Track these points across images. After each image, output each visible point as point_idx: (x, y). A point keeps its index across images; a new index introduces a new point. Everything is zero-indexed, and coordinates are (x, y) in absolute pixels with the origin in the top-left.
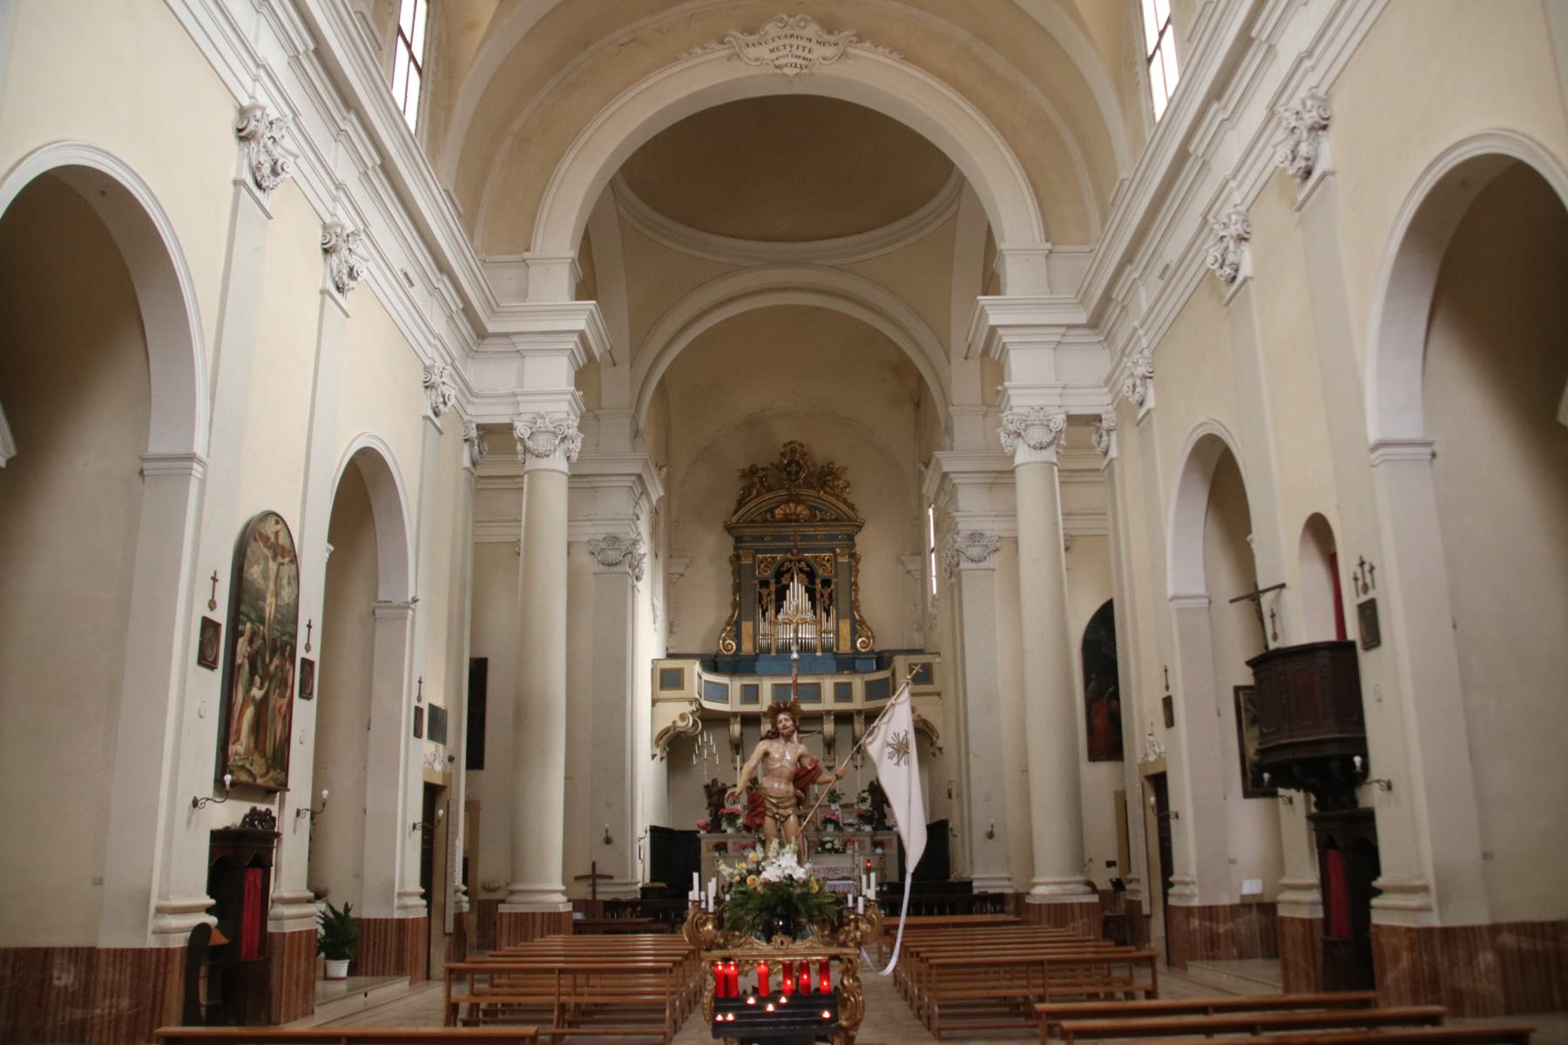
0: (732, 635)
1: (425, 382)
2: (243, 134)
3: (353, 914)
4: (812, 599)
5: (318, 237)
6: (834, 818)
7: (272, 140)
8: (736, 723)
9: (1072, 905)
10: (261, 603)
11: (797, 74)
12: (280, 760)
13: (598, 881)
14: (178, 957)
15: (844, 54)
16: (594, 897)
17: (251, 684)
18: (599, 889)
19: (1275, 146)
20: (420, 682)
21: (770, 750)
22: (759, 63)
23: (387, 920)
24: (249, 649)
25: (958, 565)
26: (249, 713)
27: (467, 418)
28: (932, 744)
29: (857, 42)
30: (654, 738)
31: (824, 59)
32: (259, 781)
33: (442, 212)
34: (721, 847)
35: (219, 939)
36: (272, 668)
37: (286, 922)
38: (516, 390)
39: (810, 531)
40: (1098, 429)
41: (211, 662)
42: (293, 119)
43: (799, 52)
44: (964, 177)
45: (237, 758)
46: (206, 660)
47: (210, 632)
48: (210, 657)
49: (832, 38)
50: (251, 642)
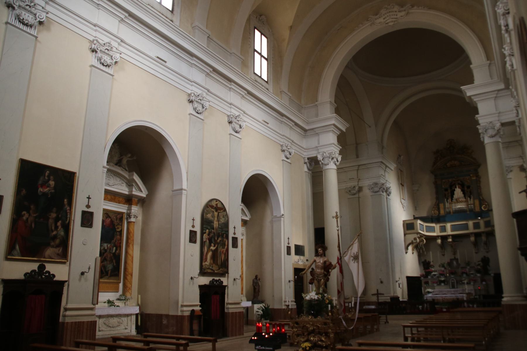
1: (281, 150)
3: (270, 307)
4: (464, 193)
5: (226, 119)
6: (466, 272)
7: (200, 100)
8: (439, 239)
10: (212, 224)
11: (394, 24)
14: (186, 318)
15: (408, 14)
16: (378, 301)
17: (210, 246)
18: (380, 298)
20: (288, 239)
21: (306, 261)
22: (380, 24)
23: (281, 309)
24: (208, 237)
26: (210, 254)
27: (304, 156)
30: (406, 247)
31: (402, 16)
32: (216, 271)
34: (427, 283)
36: (218, 241)
37: (184, 312)
41: (194, 241)
43: (393, 17)
45: (206, 266)
48: (193, 240)
49: (403, 9)
50: (209, 235)
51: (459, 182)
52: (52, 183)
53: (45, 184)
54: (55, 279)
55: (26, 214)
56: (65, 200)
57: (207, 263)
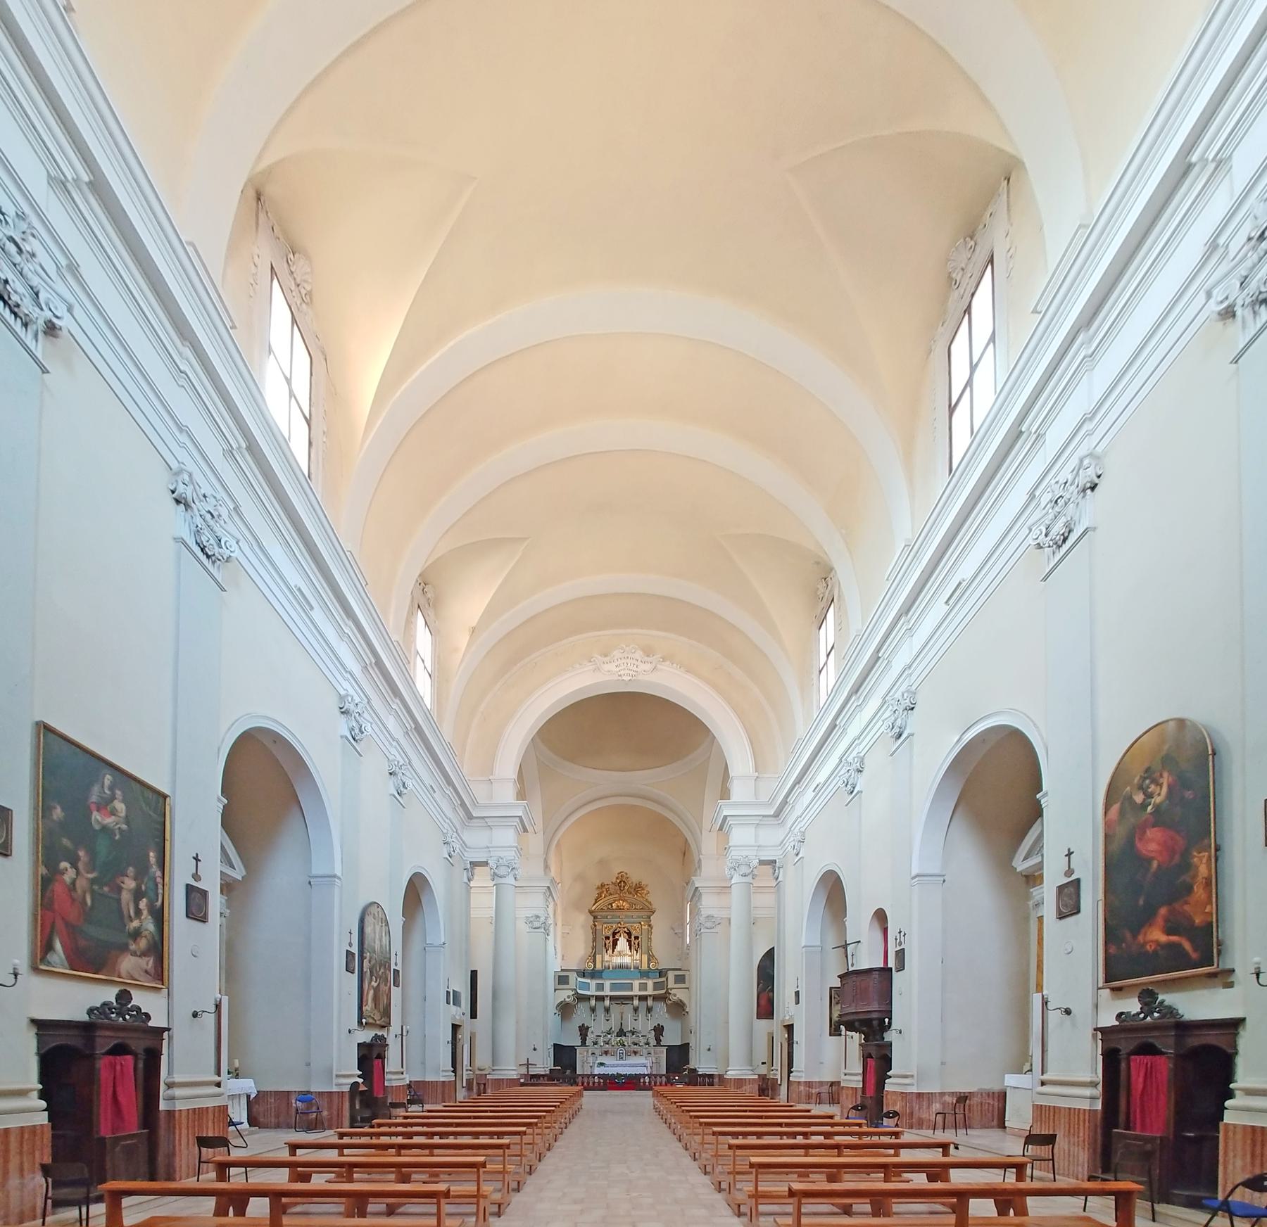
0: (592, 961)
2: (342, 710)
9: (745, 1079)
11: (630, 680)
12: (386, 1013)
13: (530, 1066)
17: (371, 979)
19: (883, 721)
25: (700, 930)
26: (371, 992)
28: (684, 1010)
29: (663, 661)
32: (378, 1022)
33: (366, 605)
35: (363, 1088)
36: (380, 973)
38: (489, 845)
39: (629, 914)
40: (774, 866)
42: (368, 703)
44: (715, 737)
46: (349, 969)
47: (350, 957)
49: (649, 659)
51: (626, 929)
52: (120, 806)
53: (105, 805)
54: (150, 1024)
55: (69, 870)
56: (152, 854)
57: (367, 1007)
